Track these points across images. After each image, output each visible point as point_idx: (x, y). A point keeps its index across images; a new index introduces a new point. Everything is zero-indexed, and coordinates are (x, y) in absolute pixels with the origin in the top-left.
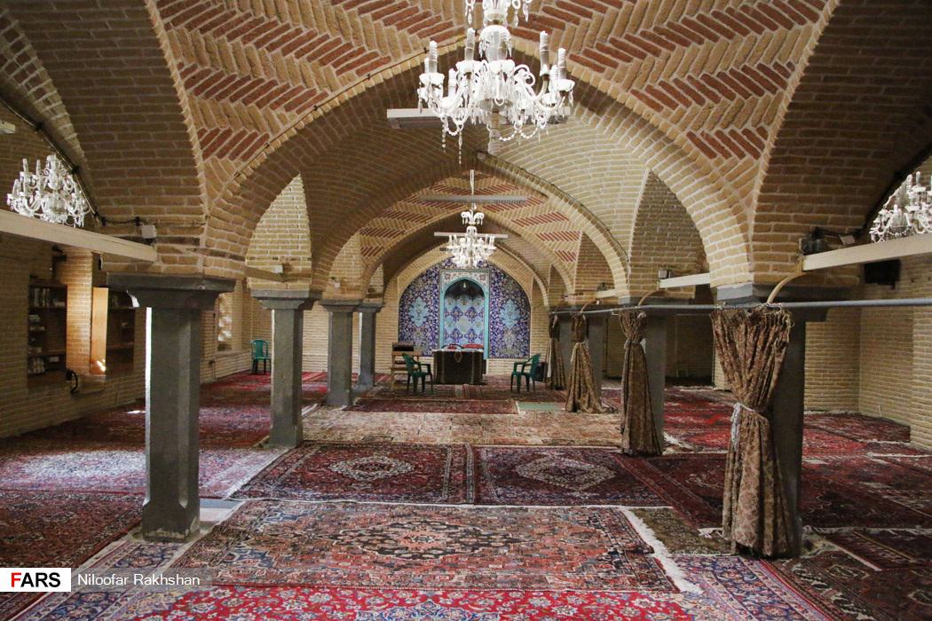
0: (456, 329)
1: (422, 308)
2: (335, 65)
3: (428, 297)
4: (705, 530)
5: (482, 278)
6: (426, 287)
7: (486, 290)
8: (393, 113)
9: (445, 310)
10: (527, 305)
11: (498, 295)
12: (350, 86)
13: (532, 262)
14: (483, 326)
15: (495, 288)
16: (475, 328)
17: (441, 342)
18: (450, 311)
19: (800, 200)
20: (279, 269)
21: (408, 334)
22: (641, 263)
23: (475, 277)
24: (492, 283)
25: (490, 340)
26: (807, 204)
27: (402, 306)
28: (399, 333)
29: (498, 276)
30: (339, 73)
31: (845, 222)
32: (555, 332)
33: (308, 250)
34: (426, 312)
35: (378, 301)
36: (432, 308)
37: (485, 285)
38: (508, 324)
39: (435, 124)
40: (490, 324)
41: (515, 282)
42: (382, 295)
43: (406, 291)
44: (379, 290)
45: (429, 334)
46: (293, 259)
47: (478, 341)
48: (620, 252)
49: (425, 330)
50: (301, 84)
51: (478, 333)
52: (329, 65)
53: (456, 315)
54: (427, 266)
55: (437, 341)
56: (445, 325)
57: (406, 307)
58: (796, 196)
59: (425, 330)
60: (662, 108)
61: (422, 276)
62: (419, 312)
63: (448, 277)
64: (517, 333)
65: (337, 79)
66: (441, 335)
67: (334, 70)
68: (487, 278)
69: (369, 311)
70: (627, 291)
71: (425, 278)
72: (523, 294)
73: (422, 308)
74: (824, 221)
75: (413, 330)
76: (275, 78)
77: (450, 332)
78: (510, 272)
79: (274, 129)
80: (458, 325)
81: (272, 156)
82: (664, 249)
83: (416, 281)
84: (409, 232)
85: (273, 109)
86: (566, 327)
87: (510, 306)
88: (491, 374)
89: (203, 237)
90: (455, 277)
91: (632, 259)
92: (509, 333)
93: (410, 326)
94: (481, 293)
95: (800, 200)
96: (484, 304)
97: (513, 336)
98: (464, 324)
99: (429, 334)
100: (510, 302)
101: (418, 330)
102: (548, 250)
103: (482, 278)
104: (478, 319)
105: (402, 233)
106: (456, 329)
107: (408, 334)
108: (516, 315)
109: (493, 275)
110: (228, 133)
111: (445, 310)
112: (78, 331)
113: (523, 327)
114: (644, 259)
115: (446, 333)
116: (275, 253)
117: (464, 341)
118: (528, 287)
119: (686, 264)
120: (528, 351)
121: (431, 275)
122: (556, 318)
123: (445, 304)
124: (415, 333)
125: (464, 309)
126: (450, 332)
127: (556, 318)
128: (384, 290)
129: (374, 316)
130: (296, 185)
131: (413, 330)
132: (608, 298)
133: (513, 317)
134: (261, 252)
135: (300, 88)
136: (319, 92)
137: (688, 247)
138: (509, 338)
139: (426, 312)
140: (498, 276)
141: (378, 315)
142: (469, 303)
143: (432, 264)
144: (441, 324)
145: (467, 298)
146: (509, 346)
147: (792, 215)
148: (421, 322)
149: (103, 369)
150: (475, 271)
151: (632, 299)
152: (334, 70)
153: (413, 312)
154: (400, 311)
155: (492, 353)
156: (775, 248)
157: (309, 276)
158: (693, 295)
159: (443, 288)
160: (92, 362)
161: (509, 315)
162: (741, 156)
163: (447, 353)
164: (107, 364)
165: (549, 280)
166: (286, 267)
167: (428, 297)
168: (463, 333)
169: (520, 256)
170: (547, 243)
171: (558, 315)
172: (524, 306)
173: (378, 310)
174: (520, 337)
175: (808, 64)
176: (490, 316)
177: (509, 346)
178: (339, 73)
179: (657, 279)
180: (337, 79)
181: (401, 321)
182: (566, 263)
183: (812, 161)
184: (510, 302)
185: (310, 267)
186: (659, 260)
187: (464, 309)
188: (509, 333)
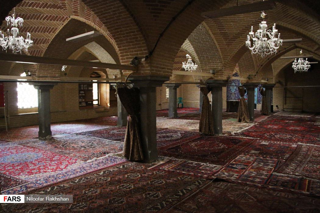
2: (47, 32)
4: (47, 137)
8: (68, 40)
19: (129, 49)
20: (114, 77)
22: (204, 68)
25: (258, 97)
26: (131, 50)
28: (227, 95)
30: (49, 34)
31: (143, 54)
46: (117, 74)
49: (235, 94)
50: (43, 38)
52: (46, 33)
58: (127, 48)
59: (235, 94)
65: (49, 35)
67: (48, 33)
74: (137, 54)
76: (43, 38)
79: (43, 49)
82: (210, 63)
85: (40, 44)
89: (37, 74)
93: (230, 92)
95: (129, 49)
110: (35, 51)
112: (104, 95)
114: (205, 67)
116: (113, 73)
119: (219, 67)
134: (110, 73)
135: (43, 39)
136: (48, 39)
137: (218, 61)
147: (129, 53)
148: (234, 91)
149: (109, 105)
152: (48, 33)
157: (121, 78)
160: (107, 104)
164: (110, 104)
166: (116, 76)
178: (49, 34)
180: (49, 35)
183: (216, 25)
185: (120, 76)
186: (210, 67)
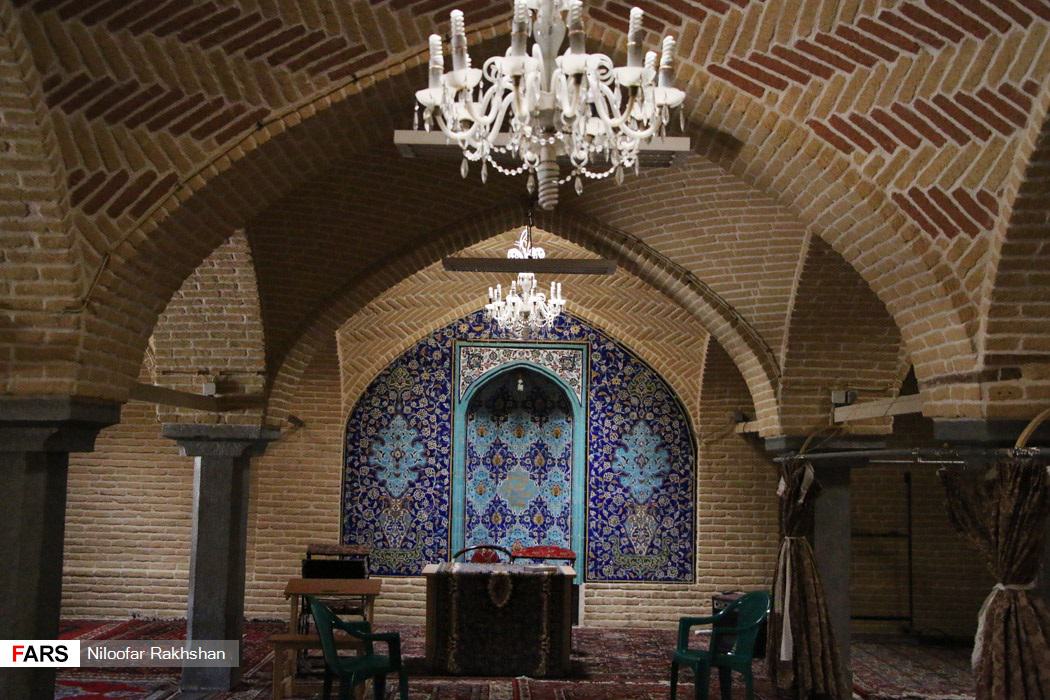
0: (497, 502)
1: (406, 446)
3: (422, 415)
5: (568, 364)
6: (418, 390)
7: (577, 396)
10: (688, 437)
11: (607, 410)
12: (312, 95)
13: (728, 297)
14: (571, 493)
17: (457, 536)
18: (481, 451)
20: (207, 389)
21: (368, 514)
23: (547, 362)
24: (593, 378)
25: (588, 533)
27: (353, 436)
28: (345, 512)
32: (797, 519)
33: (260, 357)
34: (416, 455)
35: (248, 421)
36: (433, 445)
37: (574, 382)
38: (636, 487)
39: (454, 153)
40: (587, 488)
41: (655, 377)
42: (259, 401)
43: (363, 400)
44: (253, 384)
45: (424, 516)
47: (555, 535)
48: (764, 354)
51: (555, 510)
53: (498, 463)
54: (420, 334)
55: (447, 534)
56: (468, 491)
57: (364, 443)
61: (405, 359)
62: (400, 455)
63: (475, 362)
64: (660, 512)
66: (458, 519)
68: (579, 365)
69: (220, 449)
70: (777, 427)
71: (414, 364)
72: (677, 408)
73: (406, 446)
75: (381, 503)
77: (480, 509)
78: (636, 345)
81: (189, 203)
83: (389, 372)
84: (285, 115)
86: (837, 508)
88: (592, 625)
90: (495, 361)
91: (786, 373)
92: (641, 512)
93: (374, 494)
94: (566, 408)
96: (575, 433)
97: (650, 520)
98: (519, 488)
99: (424, 516)
100: (641, 431)
101: (396, 504)
102: (865, 190)
103: (568, 364)
104: (556, 474)
105: (258, 120)
106: (497, 502)
107: (368, 514)
108: (657, 463)
111: (469, 450)
113: (676, 497)
115: (469, 510)
117: (519, 536)
118: (689, 387)
120: (692, 561)
121: (431, 358)
122: (810, 472)
123: (467, 435)
124: (385, 513)
125: (519, 448)
126: (480, 509)
127: (810, 472)
128: (269, 385)
129: (241, 463)
130: (237, 247)
131: (381, 503)
132: (860, 422)
133: (651, 469)
138: (640, 525)
139: (416, 455)
140: (611, 362)
141: (264, 466)
142: (532, 434)
144: (458, 489)
145: (527, 418)
146: (641, 548)
148: (403, 481)
150: (546, 345)
151: (788, 440)
153: (383, 456)
154: (347, 453)
155: (596, 566)
156: (109, 530)
158: (889, 428)
159: (464, 393)
161: (638, 467)
162: (960, 194)
163: (463, 577)
165: (782, 356)
167: (422, 415)
168: (517, 511)
169: (689, 279)
170: (859, 162)
171: (815, 463)
172: (677, 441)
173: (257, 446)
174: (668, 523)
176: (589, 466)
177: (641, 548)
179: (828, 406)
181: (350, 482)
182: (941, 245)
184: (641, 431)
187: (519, 448)
188: (641, 512)
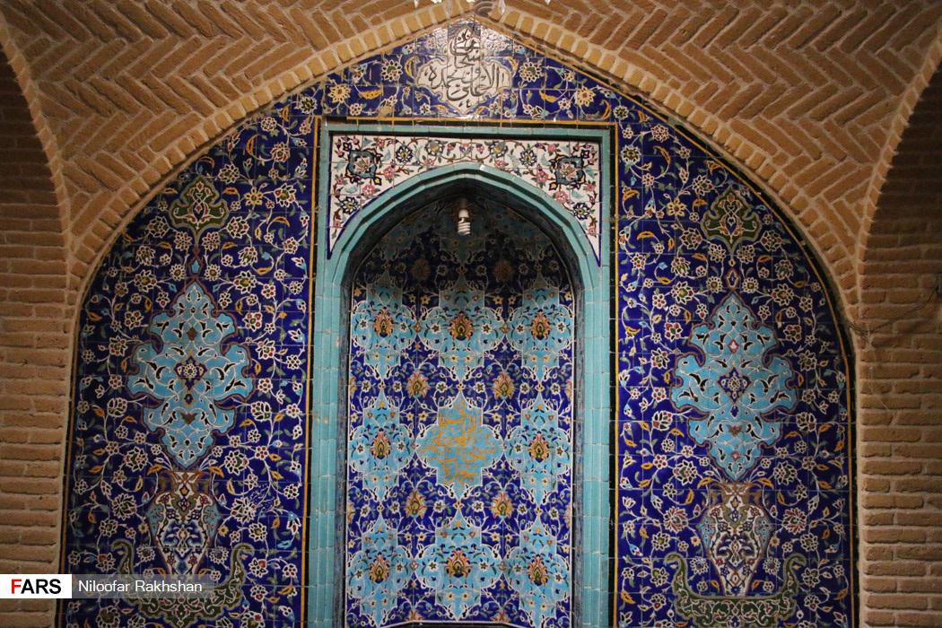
0: (414, 471)
7: (590, 242)
9: (352, 360)
15: (644, 236)
16: (520, 461)
18: (382, 365)
21: (123, 505)
23: (521, 167)
24: (626, 200)
25: (618, 547)
27: (95, 330)
28: (72, 500)
29: (663, 166)
36: (267, 350)
37: (583, 211)
41: (759, 199)
49: (222, 485)
51: (539, 488)
57: (117, 347)
59: (222, 485)
60: (851, 83)
61: (211, 160)
63: (364, 167)
64: (776, 498)
66: (323, 515)
68: (593, 173)
71: (230, 174)
72: (808, 269)
77: (379, 487)
78: (719, 130)
80: (430, 446)
83: (177, 188)
87: (732, 336)
90: (406, 168)
92: (735, 498)
97: (755, 517)
100: (731, 314)
101: (185, 483)
104: (539, 415)
106: (414, 471)
109: (631, 158)
111: (352, 360)
124: (162, 504)
125: (462, 359)
126: (379, 487)
133: (757, 402)
142: (488, 332)
143: (267, 91)
145: (476, 298)
148: (201, 432)
153: (157, 374)
154: (81, 369)
161: (726, 397)
168: (458, 491)
174: (796, 522)
175: (884, 180)
176: (618, 397)
181: (86, 431)
184: (731, 314)
187: (462, 359)
